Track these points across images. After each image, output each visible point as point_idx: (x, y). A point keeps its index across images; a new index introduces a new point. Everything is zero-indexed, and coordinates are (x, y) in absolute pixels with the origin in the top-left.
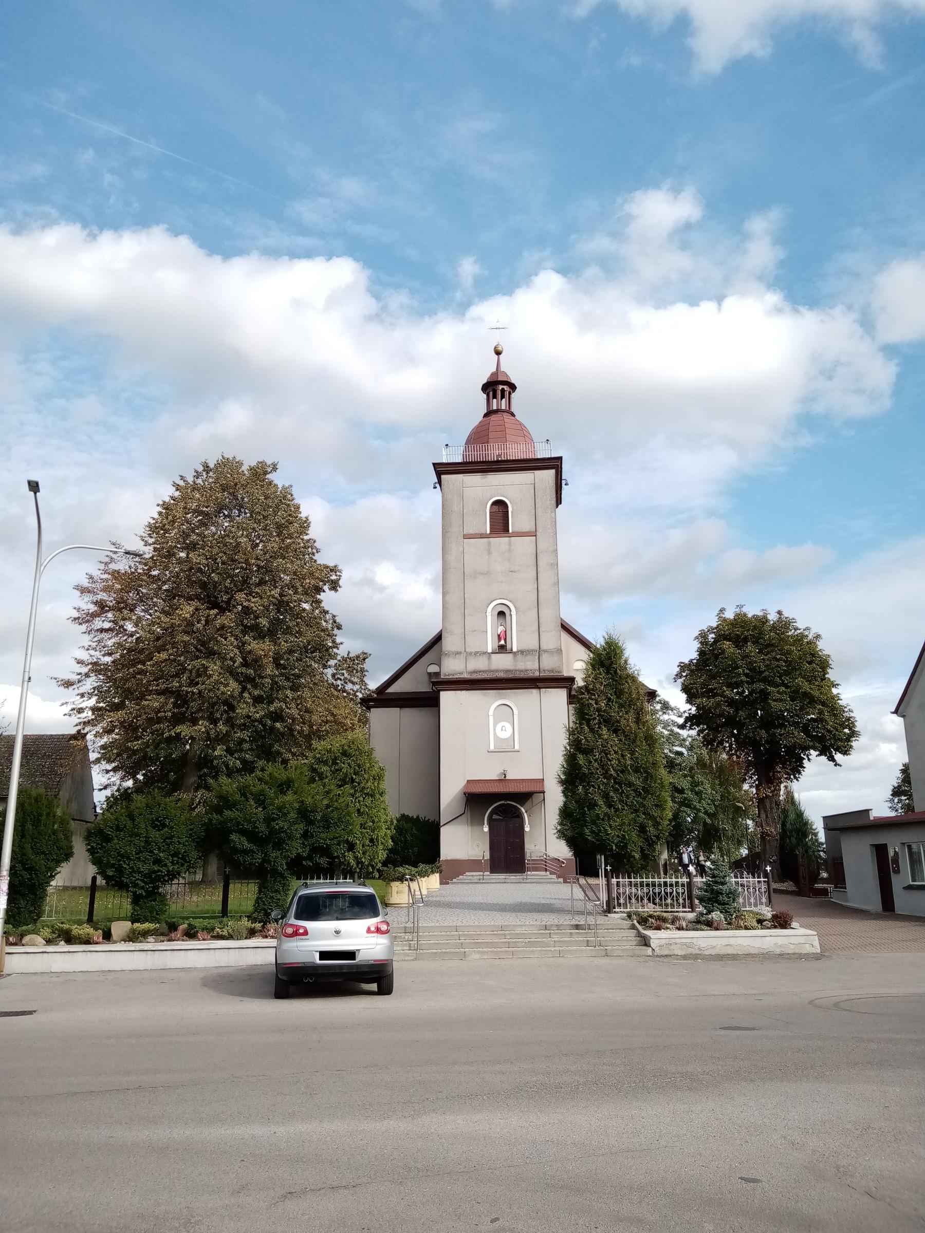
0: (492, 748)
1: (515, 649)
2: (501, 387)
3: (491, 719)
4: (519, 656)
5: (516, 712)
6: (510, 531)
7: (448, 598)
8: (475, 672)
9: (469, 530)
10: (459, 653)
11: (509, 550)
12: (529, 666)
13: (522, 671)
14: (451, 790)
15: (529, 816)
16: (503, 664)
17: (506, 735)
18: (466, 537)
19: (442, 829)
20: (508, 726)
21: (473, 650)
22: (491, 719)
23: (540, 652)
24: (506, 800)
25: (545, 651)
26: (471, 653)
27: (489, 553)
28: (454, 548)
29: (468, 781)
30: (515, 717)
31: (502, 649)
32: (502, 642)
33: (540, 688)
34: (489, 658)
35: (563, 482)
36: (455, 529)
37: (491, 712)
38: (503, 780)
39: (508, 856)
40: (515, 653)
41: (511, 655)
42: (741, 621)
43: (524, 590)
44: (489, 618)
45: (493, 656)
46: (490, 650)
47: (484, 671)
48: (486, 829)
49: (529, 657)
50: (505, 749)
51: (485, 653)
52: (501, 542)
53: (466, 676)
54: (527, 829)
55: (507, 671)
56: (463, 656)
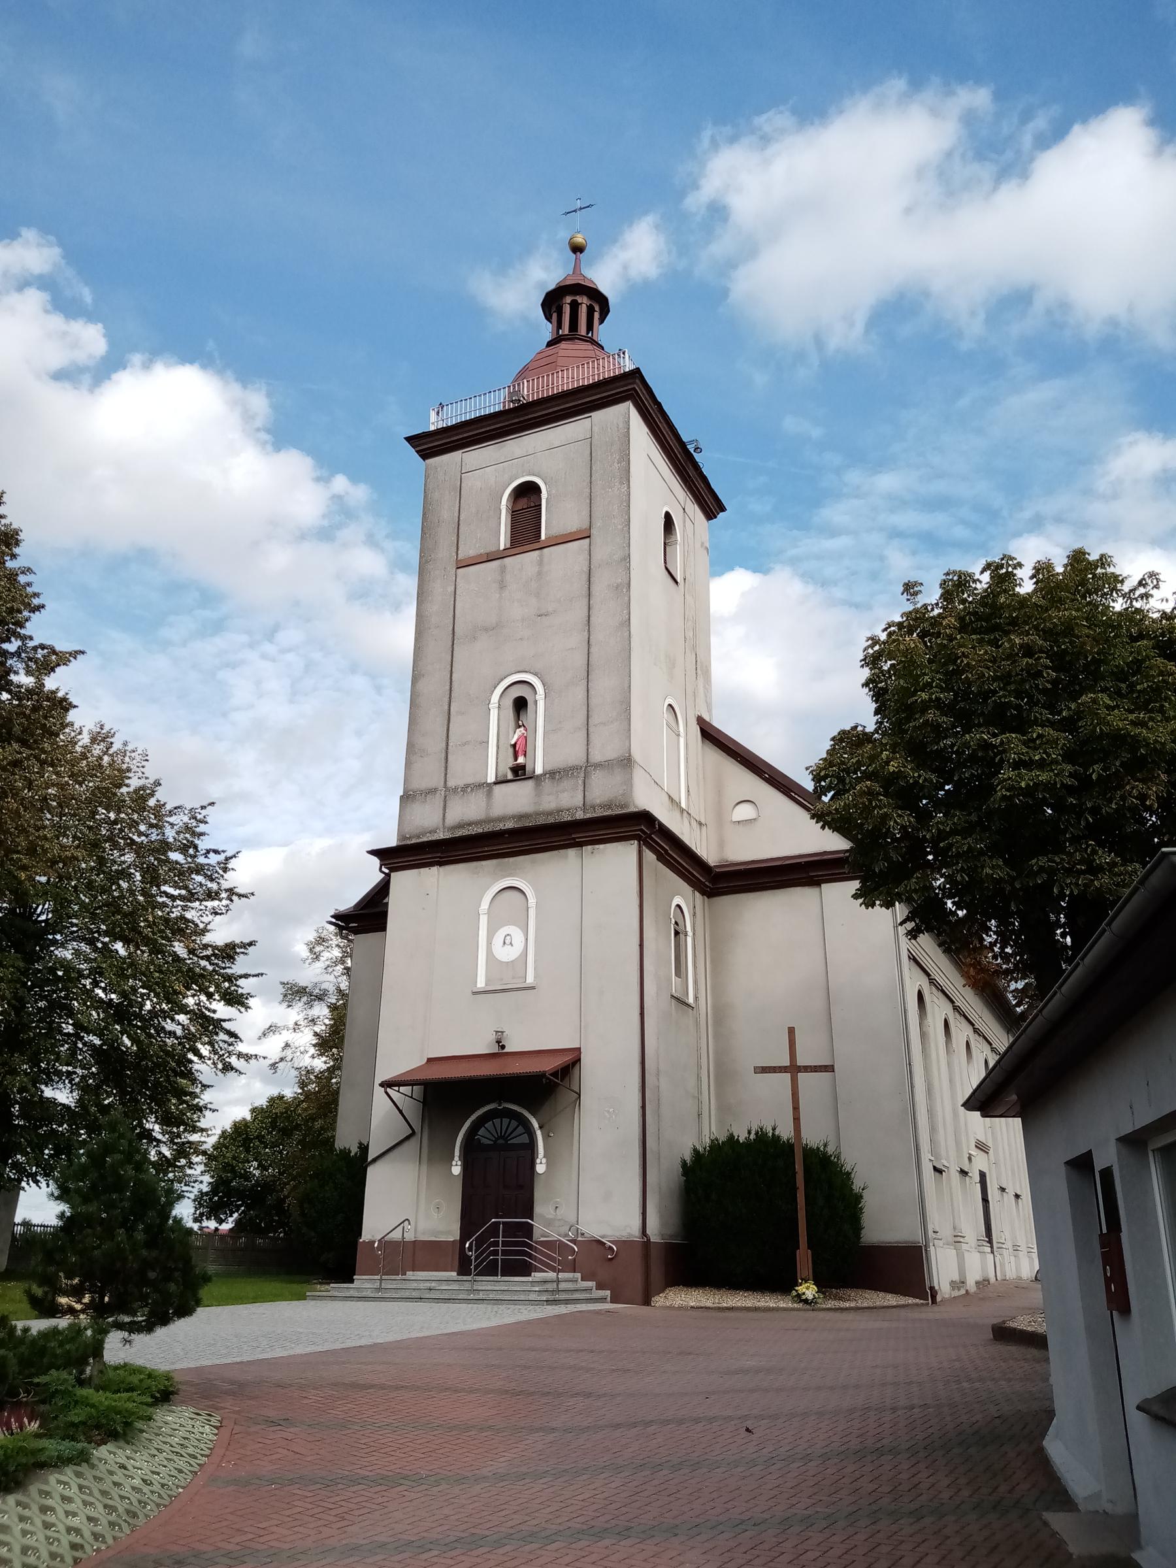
0: (481, 984)
1: (539, 770)
2: (568, 299)
3: (484, 920)
4: (547, 784)
5: (532, 901)
6: (543, 537)
7: (421, 685)
8: (460, 826)
9: (469, 550)
10: (432, 791)
11: (539, 573)
12: (565, 801)
13: (550, 813)
14: (378, 1081)
15: (546, 1137)
16: (516, 802)
17: (506, 954)
18: (462, 565)
19: (369, 1169)
20: (517, 934)
21: (461, 783)
22: (484, 920)
23: (584, 770)
24: (501, 1099)
25: (598, 766)
26: (455, 790)
27: (502, 586)
28: (440, 589)
29: (429, 1060)
30: (532, 913)
31: (519, 772)
32: (521, 760)
33: (580, 845)
34: (489, 794)
35: (691, 448)
36: (444, 553)
37: (485, 905)
38: (500, 1053)
39: (497, 1230)
40: (539, 777)
41: (529, 784)
42: (543, 305)
43: (562, 647)
44: (494, 714)
45: (497, 788)
46: (491, 778)
47: (470, 824)
48: (457, 1170)
49: (566, 784)
50: (507, 987)
51: (480, 786)
52: (528, 560)
53: (441, 835)
54: (540, 1168)
55: (521, 817)
56: (438, 800)
